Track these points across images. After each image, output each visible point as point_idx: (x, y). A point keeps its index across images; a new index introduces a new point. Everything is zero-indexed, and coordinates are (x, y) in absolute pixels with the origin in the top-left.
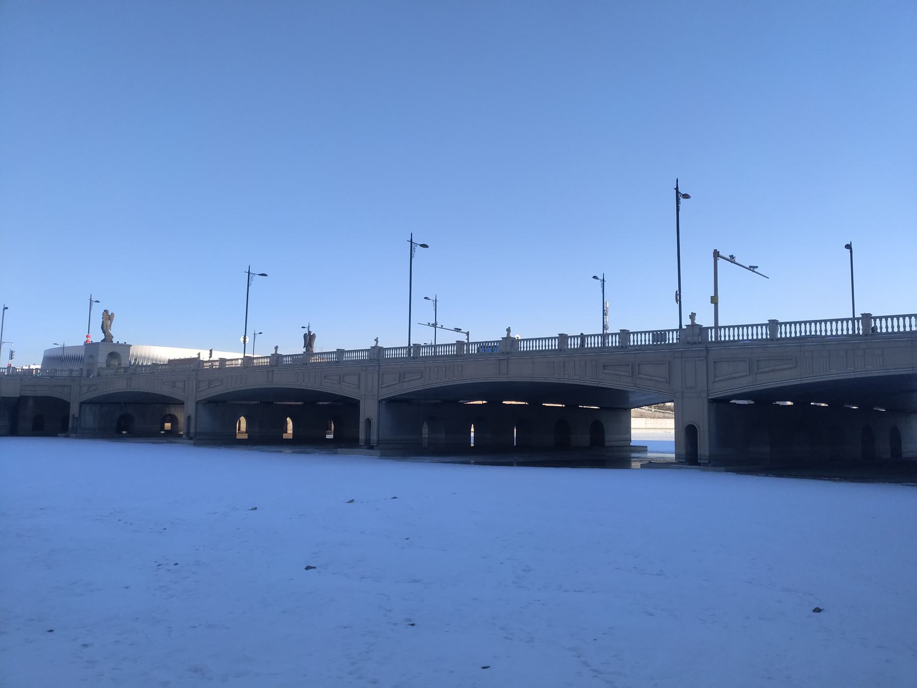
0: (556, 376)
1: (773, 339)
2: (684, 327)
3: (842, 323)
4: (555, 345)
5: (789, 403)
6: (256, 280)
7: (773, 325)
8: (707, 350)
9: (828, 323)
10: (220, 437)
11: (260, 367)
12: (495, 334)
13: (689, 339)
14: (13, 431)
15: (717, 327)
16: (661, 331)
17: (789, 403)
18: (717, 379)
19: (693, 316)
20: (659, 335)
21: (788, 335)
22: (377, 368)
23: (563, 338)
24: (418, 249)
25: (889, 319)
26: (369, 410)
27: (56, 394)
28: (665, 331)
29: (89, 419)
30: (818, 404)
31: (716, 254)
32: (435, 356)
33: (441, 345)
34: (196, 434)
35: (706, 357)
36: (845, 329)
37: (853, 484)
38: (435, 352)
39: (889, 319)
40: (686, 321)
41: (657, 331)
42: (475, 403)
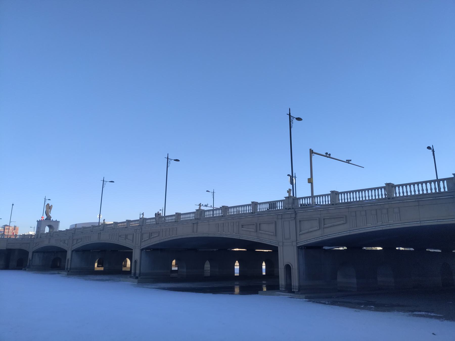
0: (380, 223)
1: (390, 198)
2: (100, 224)
3: (418, 185)
4: (382, 194)
5: (379, 248)
6: (172, 163)
7: (390, 187)
8: (296, 214)
9: (416, 185)
10: (85, 272)
11: (187, 221)
12: (193, 208)
13: (287, 206)
14: (7, 267)
15: (313, 197)
16: (273, 202)
17: (379, 248)
18: (303, 232)
19: (104, 220)
20: (273, 204)
21: (355, 200)
22: (293, 216)
23: (255, 204)
24: (172, 163)
25: (416, 185)
26: (288, 256)
27: (23, 247)
28: (275, 201)
29: (37, 261)
30: (374, 248)
31: (312, 152)
32: (213, 217)
33: (320, 196)
34: (70, 269)
35: (295, 218)
36: (431, 189)
37: (379, 312)
38: (213, 214)
39: (420, 185)
40: (102, 221)
41: (271, 202)
42: (267, 251)
